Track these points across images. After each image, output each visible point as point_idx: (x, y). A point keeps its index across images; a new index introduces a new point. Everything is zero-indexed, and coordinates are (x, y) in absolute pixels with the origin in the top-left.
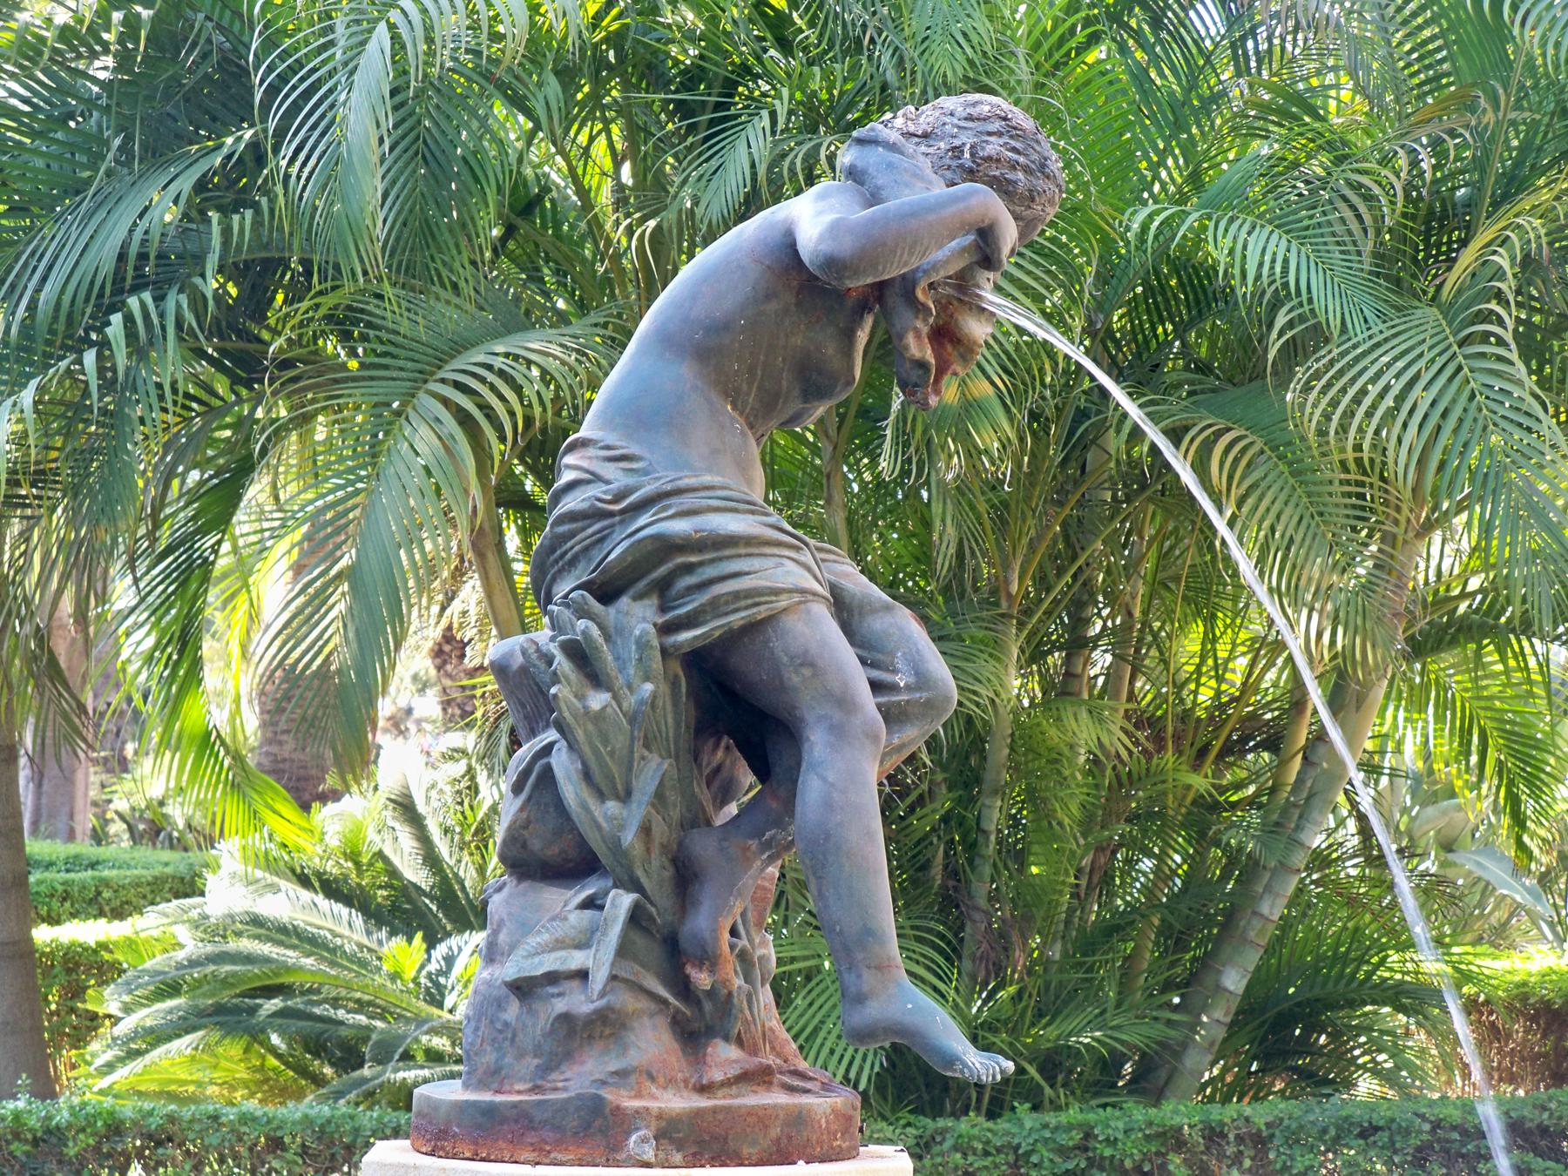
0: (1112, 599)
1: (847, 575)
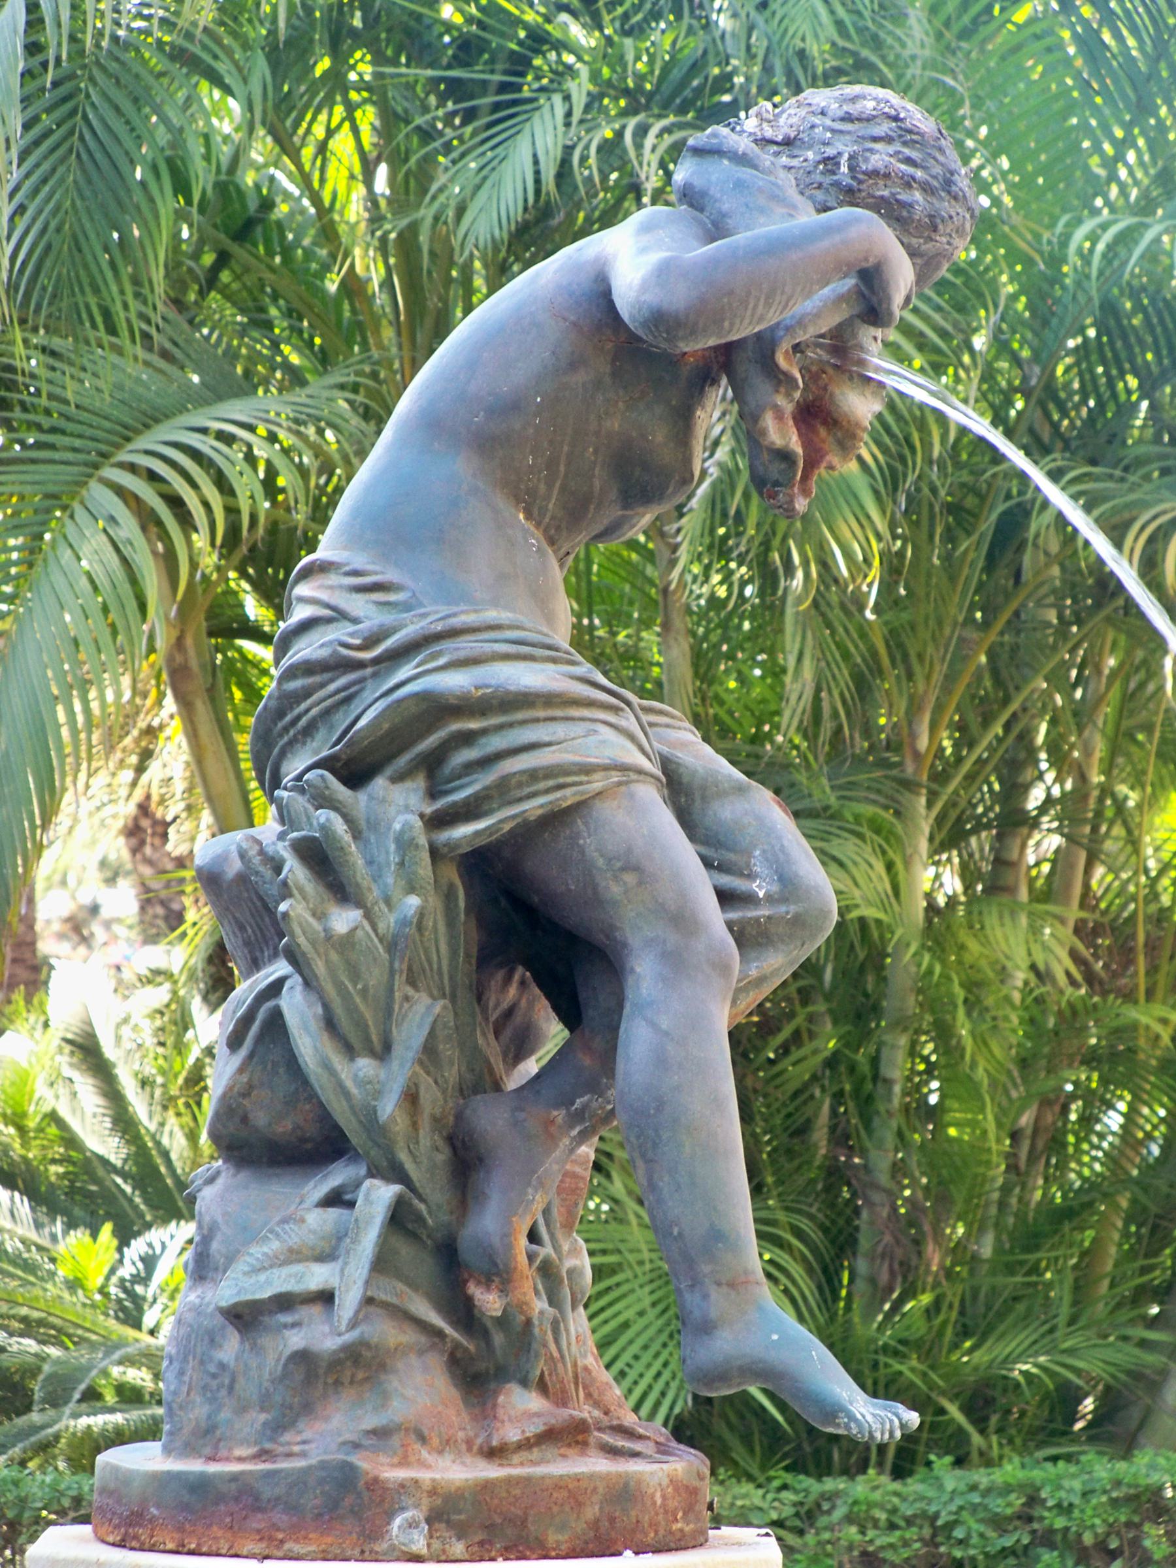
0: (1059, 759)
1: (684, 745)
